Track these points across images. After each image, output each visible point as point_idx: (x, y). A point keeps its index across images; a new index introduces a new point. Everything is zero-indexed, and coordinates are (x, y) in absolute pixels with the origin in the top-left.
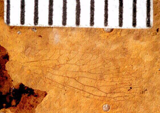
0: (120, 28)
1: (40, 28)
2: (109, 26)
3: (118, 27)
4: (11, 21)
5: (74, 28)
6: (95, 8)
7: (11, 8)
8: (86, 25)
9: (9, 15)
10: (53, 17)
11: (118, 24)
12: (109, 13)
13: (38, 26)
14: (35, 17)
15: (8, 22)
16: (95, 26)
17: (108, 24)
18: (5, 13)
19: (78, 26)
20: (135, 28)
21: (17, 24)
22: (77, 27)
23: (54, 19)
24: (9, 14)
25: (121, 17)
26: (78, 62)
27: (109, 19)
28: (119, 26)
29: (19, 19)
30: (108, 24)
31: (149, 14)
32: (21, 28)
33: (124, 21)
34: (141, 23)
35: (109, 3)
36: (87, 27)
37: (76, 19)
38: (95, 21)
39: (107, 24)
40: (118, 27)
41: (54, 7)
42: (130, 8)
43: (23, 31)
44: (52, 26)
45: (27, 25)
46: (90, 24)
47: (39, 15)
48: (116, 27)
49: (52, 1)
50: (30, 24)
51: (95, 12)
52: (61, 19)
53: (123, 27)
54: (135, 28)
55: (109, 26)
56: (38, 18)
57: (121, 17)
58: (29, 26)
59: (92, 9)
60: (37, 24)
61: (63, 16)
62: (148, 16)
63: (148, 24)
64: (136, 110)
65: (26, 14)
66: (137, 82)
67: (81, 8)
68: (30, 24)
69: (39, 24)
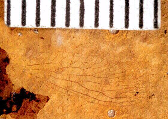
0: (126, 29)
1: (42, 29)
2: (114, 27)
3: (124, 29)
4: (12, 22)
5: (78, 30)
6: (100, 8)
7: (11, 9)
8: (91, 27)
9: (10, 16)
10: (56, 18)
11: (124, 25)
12: (114, 13)
13: (40, 27)
14: (37, 18)
15: (9, 23)
16: (100, 28)
17: (114, 26)
18: (6, 14)
19: (82, 27)
20: (142, 30)
21: (18, 26)
22: (81, 28)
23: (56, 20)
24: (10, 14)
25: (127, 18)
26: (82, 65)
27: (114, 20)
28: (124, 28)
29: (20, 20)
30: (114, 26)
31: (157, 15)
32: (22, 29)
33: (130, 22)
34: (148, 24)
35: (114, 3)
36: (91, 28)
37: (80, 20)
38: (100, 22)
39: (112, 25)
40: (124, 29)
41: (57, 8)
42: (136, 9)
43: (24, 32)
44: (54, 28)
45: (28, 26)
46: (95, 25)
47: (41, 16)
48: (122, 28)
49: (55, 1)
50: (32, 25)
51: (100, 13)
52: (64, 20)
53: (129, 29)
54: (142, 30)
55: (114, 27)
56: (39, 19)
57: (127, 18)
58: (30, 27)
59: (97, 9)
60: (39, 25)
61: (66, 17)
62: (156, 17)
63: (156, 25)
64: (143, 116)
65: (27, 14)
66: (144, 87)
67: (85, 8)
68: (31, 26)
69: (41, 25)
